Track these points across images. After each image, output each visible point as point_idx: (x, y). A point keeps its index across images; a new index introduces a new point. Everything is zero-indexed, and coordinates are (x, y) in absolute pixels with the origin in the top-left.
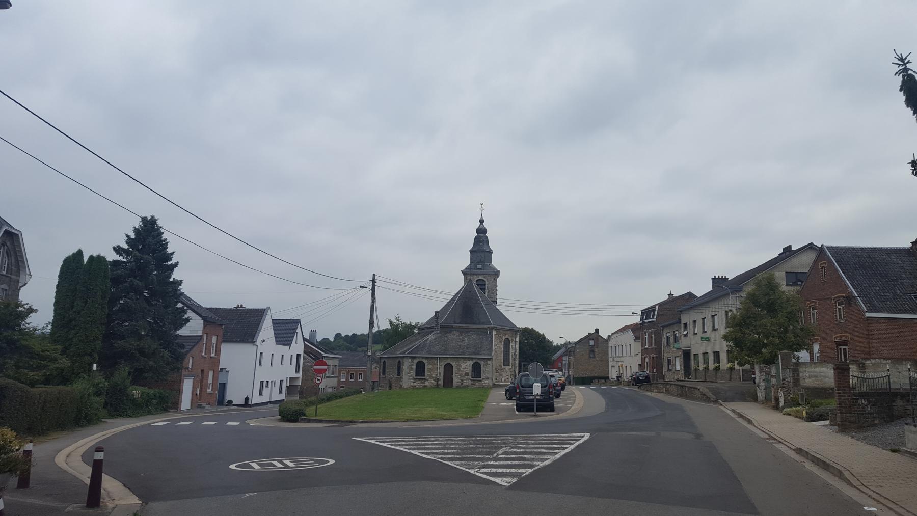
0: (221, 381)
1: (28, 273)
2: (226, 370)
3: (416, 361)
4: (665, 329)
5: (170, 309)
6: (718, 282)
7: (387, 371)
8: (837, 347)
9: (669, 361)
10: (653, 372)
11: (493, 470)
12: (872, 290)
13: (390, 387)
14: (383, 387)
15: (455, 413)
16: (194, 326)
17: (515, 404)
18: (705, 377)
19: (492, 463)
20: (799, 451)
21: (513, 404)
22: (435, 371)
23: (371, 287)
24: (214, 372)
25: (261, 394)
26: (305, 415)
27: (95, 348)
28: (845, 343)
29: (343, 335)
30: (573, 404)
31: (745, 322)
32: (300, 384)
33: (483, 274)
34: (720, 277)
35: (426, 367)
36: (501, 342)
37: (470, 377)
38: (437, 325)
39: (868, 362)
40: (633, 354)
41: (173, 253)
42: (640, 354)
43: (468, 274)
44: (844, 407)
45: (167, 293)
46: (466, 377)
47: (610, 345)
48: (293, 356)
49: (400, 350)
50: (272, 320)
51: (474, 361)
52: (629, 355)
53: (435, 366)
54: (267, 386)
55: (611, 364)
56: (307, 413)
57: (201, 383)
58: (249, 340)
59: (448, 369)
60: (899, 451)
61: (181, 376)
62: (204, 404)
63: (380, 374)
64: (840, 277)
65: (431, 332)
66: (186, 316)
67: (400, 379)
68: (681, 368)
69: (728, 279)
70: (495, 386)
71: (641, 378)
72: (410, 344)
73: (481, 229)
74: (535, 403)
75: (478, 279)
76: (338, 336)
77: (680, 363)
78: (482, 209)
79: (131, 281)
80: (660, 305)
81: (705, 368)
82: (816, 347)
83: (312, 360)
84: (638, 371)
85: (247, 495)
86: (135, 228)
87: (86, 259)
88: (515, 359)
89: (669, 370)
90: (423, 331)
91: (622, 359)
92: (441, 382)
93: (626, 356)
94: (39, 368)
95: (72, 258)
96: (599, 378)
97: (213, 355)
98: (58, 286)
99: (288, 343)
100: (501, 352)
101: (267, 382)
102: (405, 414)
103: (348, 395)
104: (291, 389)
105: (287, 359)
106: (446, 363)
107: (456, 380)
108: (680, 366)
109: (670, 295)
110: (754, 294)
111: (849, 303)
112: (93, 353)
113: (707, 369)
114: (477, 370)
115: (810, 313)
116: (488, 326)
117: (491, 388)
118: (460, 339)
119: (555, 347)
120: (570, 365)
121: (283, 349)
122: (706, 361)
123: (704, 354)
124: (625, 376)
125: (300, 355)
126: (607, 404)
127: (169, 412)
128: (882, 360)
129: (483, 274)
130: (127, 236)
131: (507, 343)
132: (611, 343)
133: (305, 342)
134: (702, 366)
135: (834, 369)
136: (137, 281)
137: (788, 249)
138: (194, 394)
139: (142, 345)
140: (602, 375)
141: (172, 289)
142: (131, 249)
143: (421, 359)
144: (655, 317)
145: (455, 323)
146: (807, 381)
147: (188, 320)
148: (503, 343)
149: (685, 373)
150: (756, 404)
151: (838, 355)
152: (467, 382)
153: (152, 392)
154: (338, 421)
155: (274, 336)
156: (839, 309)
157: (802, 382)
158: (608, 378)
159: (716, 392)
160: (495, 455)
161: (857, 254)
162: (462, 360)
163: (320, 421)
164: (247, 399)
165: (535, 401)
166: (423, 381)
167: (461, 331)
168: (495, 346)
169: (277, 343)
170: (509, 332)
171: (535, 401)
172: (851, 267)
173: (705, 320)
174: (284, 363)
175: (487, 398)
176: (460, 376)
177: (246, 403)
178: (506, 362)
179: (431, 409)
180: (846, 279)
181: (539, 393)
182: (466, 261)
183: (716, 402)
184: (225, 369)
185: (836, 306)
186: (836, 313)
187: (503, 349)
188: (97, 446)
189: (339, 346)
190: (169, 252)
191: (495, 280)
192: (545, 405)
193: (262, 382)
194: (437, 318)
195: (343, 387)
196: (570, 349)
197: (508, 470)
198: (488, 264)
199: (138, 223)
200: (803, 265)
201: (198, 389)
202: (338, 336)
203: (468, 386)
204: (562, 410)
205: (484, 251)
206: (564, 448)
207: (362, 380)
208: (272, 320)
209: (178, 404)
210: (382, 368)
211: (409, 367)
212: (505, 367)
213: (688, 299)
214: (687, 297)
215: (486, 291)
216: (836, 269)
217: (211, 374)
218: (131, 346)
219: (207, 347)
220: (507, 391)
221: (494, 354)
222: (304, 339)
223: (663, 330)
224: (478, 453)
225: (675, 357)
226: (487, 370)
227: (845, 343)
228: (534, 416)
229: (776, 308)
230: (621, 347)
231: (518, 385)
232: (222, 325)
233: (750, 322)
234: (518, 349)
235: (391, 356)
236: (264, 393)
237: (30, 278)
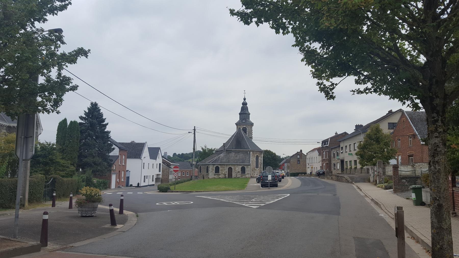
0: (127, 176)
1: (41, 128)
2: (129, 171)
3: (215, 166)
4: (333, 150)
5: (106, 144)
6: (358, 127)
7: (201, 171)
8: (409, 158)
9: (334, 165)
10: (327, 170)
11: (250, 204)
12: (425, 131)
13: (204, 178)
14: (200, 178)
15: (234, 188)
16: (116, 152)
17: (261, 184)
18: (350, 172)
19: (250, 202)
20: (372, 200)
21: (260, 184)
22: (224, 171)
23: (193, 133)
24: (124, 172)
25: (144, 181)
26: (170, 189)
27: (75, 162)
28: (412, 156)
29: (177, 154)
30: (286, 184)
31: (365, 147)
32: (161, 177)
33: (246, 125)
34: (359, 125)
35: (220, 169)
36: (254, 157)
37: (240, 173)
38: (224, 150)
39: (416, 164)
40: (318, 162)
41: (105, 119)
42: (321, 162)
43: (238, 125)
44: (396, 183)
45: (104, 137)
46: (238, 173)
47: (307, 158)
48: (158, 164)
49: (208, 161)
50: (148, 148)
51: (242, 166)
52: (314, 162)
53: (224, 168)
54: (147, 178)
55: (307, 166)
56: (170, 188)
57: (119, 177)
58: (138, 157)
59: (230, 170)
60: (409, 199)
61: (111, 173)
62: (121, 186)
63: (198, 172)
64: (411, 125)
65: (222, 153)
66: (113, 147)
67: (208, 174)
68: (340, 168)
69: (363, 126)
70: (252, 177)
71: (321, 173)
72: (212, 158)
73: (244, 103)
74: (269, 183)
75: (243, 127)
76: (175, 154)
77: (339, 166)
78: (245, 93)
79: (89, 132)
80: (331, 138)
81: (350, 168)
82: (400, 158)
83: (166, 166)
84: (320, 169)
85: (169, 211)
86: (88, 107)
87: (68, 123)
88: (261, 165)
89: (334, 169)
90: (218, 152)
91: (313, 164)
92: (227, 176)
93: (315, 163)
94: (63, 171)
95: (62, 122)
96: (301, 173)
97: (123, 164)
98: (57, 135)
99: (156, 159)
100: (255, 162)
101: (147, 176)
102: (213, 189)
103: (185, 182)
104: (157, 180)
105: (155, 166)
106: (229, 167)
107: (234, 175)
108: (339, 167)
109: (336, 133)
110: (370, 134)
111: (414, 138)
112: (74, 164)
113: (351, 168)
114: (243, 170)
115: (397, 142)
116: (248, 150)
117: (250, 178)
118: (235, 156)
119: (281, 159)
120: (288, 167)
121: (153, 161)
122: (351, 165)
123: (350, 161)
124: (314, 172)
125: (161, 164)
126: (302, 184)
127: (107, 189)
128: (423, 163)
129: (246, 125)
130: (85, 111)
131: (257, 158)
132: (307, 157)
133: (163, 158)
134: (349, 167)
135: (393, 168)
136: (91, 132)
137: (390, 112)
138: (116, 182)
139: (95, 160)
140: (304, 172)
141: (107, 135)
142: (87, 117)
143: (217, 165)
144: (328, 144)
145: (233, 149)
146: (389, 173)
147: (114, 149)
148: (255, 158)
149: (341, 170)
150: (369, 183)
151: (409, 160)
152: (239, 175)
153: (101, 180)
154: (185, 192)
155: (149, 155)
156: (410, 140)
157: (387, 174)
158: (306, 173)
159: (352, 179)
160: (251, 201)
161: (420, 114)
162: (236, 165)
163: (177, 192)
164: (138, 184)
165: (269, 183)
166: (218, 175)
167: (236, 152)
168: (251, 159)
169: (151, 158)
170: (258, 152)
171: (269, 183)
172: (416, 121)
173: (351, 145)
174: (154, 168)
175: (248, 182)
176: (236, 173)
177: (138, 186)
178: (257, 166)
179: (223, 187)
180: (413, 127)
181: (271, 179)
182: (237, 119)
183: (352, 183)
184: (129, 170)
185: (409, 139)
186: (409, 142)
187: (255, 161)
188: (122, 194)
189: (175, 159)
190: (104, 118)
191: (251, 127)
192: (274, 184)
193: (145, 176)
194: (225, 147)
195: (180, 179)
196: (288, 159)
197: (256, 204)
198: (248, 120)
199: (89, 105)
200: (395, 119)
201: (118, 179)
202: (175, 154)
203: (239, 177)
204: (282, 186)
205: (246, 114)
206: (278, 199)
207: (188, 175)
208: (148, 148)
209: (110, 186)
210: (199, 170)
211: (212, 169)
212: (256, 169)
213: (345, 135)
214: (344, 134)
215: (247, 133)
216: (409, 122)
217: (123, 172)
218: (90, 161)
219: (121, 161)
220: (257, 179)
221: (251, 163)
222: (162, 157)
223: (332, 150)
224: (245, 200)
225: (337, 163)
226: (248, 170)
227: (412, 156)
228: (269, 189)
229: (380, 140)
230: (312, 158)
231: (262, 176)
232: (126, 151)
233: (367, 147)
234: (262, 160)
235: (203, 164)
236: (145, 181)
237: (43, 131)
